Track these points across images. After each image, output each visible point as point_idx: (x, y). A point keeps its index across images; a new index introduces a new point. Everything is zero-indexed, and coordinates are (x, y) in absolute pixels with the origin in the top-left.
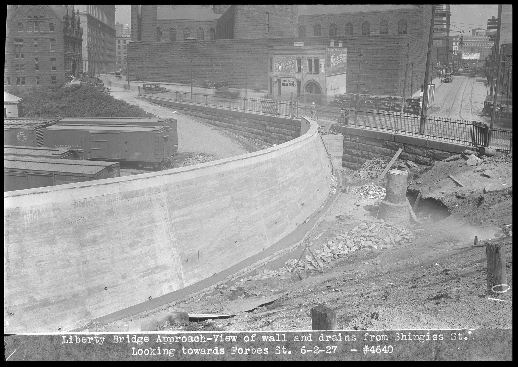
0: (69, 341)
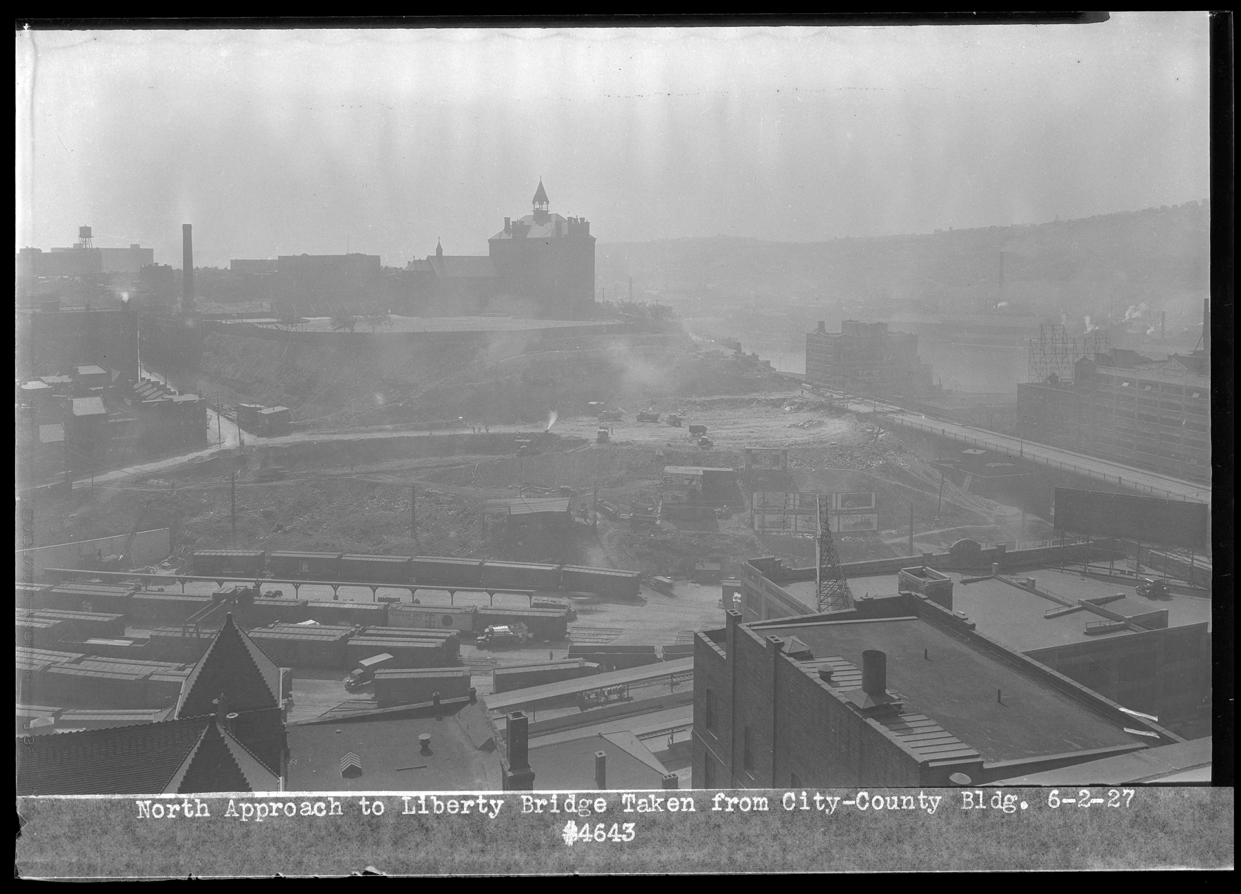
0: (196, 812)
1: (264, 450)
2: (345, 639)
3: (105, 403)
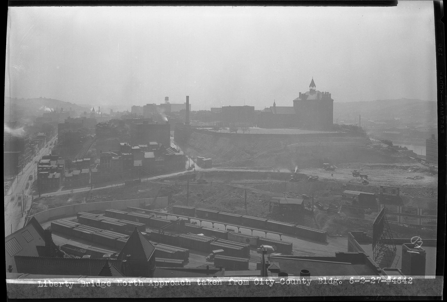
1: (202, 173)
2: (210, 242)
3: (154, 154)
